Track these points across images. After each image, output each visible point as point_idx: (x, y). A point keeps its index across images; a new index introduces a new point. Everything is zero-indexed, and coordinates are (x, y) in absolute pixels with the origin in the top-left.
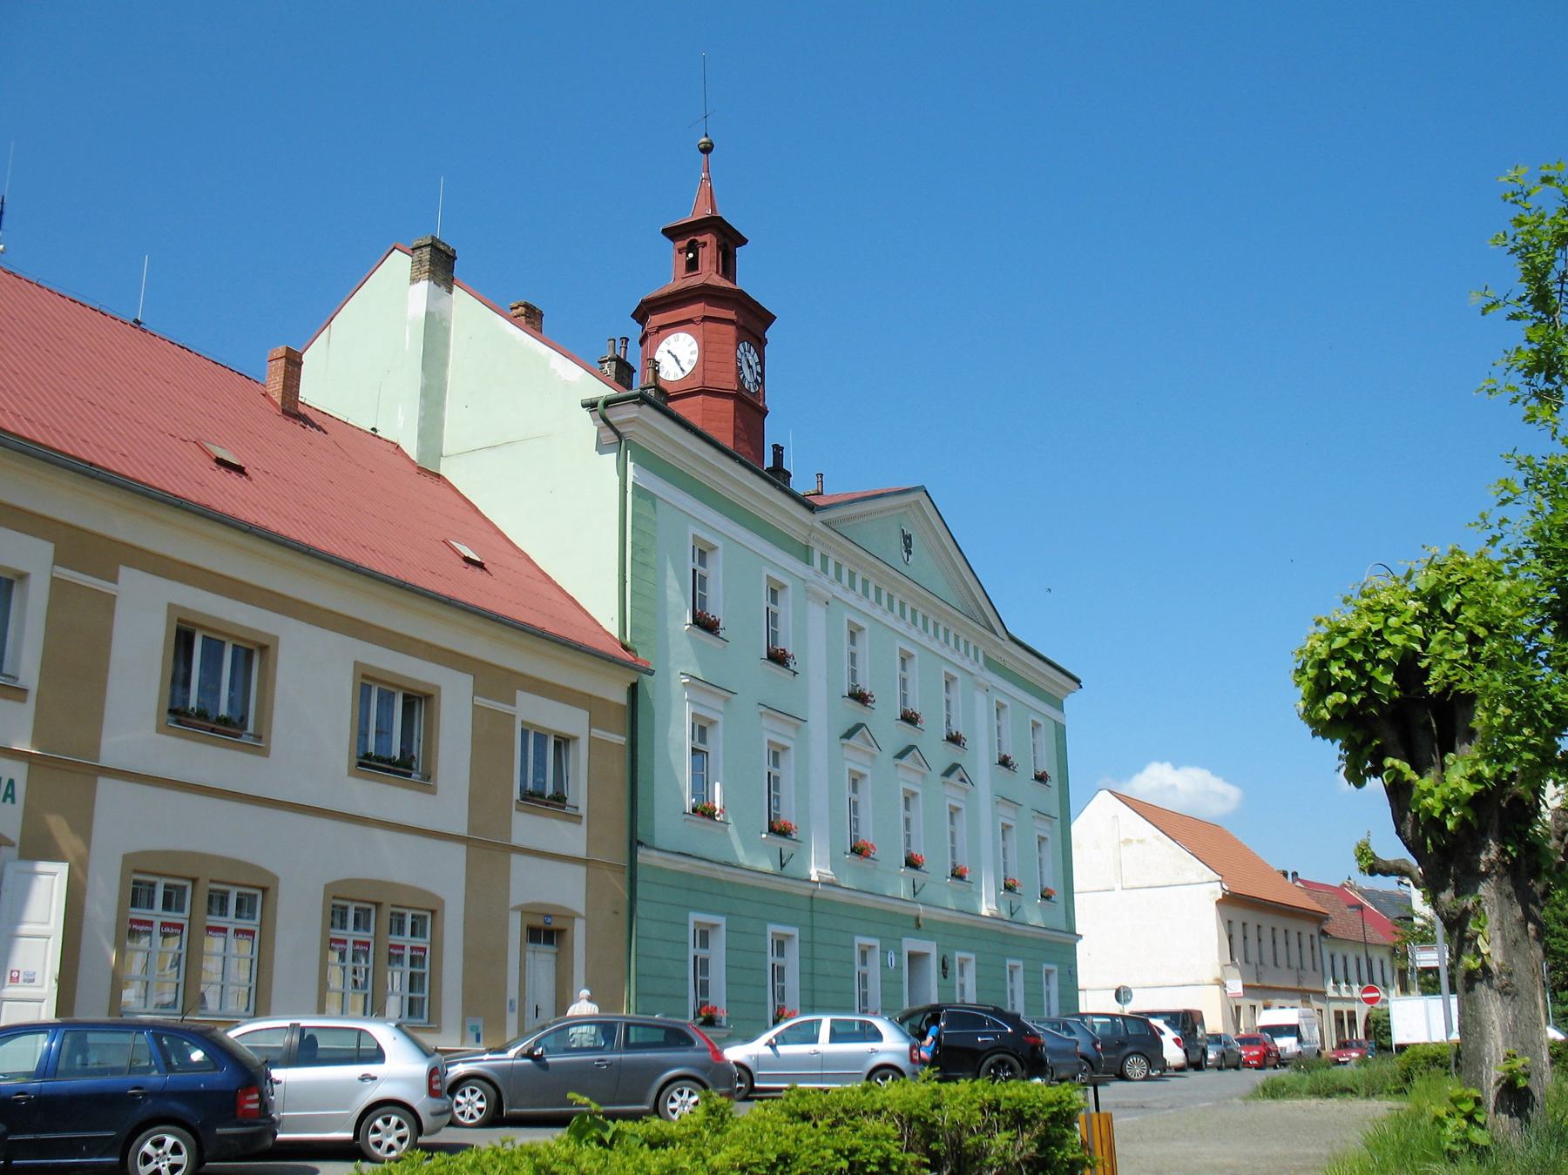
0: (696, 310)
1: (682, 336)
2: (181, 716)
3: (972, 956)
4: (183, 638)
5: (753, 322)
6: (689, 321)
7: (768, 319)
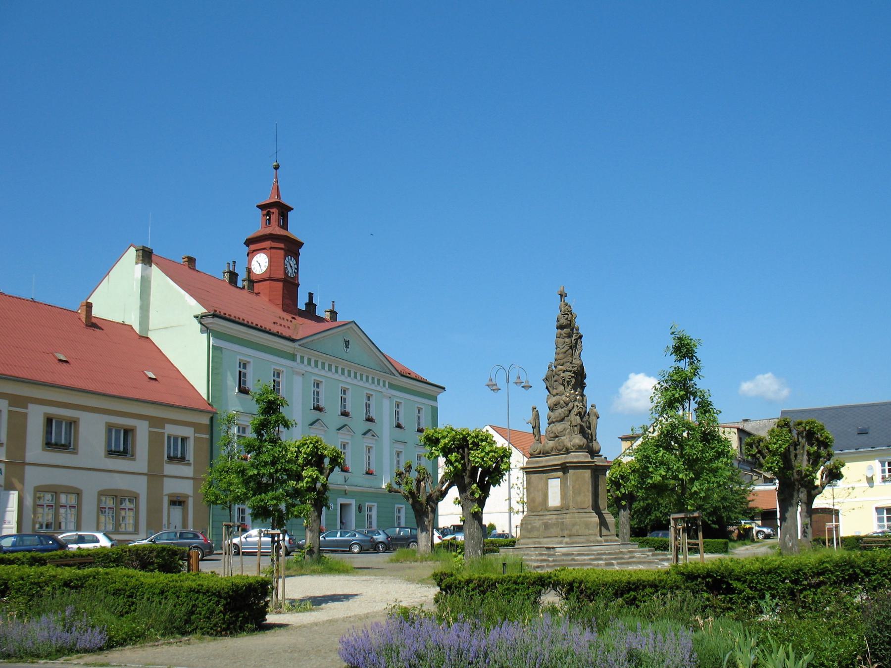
0: (268, 244)
1: (262, 255)
4: (49, 421)
5: (293, 247)
6: (265, 249)
7: (300, 244)
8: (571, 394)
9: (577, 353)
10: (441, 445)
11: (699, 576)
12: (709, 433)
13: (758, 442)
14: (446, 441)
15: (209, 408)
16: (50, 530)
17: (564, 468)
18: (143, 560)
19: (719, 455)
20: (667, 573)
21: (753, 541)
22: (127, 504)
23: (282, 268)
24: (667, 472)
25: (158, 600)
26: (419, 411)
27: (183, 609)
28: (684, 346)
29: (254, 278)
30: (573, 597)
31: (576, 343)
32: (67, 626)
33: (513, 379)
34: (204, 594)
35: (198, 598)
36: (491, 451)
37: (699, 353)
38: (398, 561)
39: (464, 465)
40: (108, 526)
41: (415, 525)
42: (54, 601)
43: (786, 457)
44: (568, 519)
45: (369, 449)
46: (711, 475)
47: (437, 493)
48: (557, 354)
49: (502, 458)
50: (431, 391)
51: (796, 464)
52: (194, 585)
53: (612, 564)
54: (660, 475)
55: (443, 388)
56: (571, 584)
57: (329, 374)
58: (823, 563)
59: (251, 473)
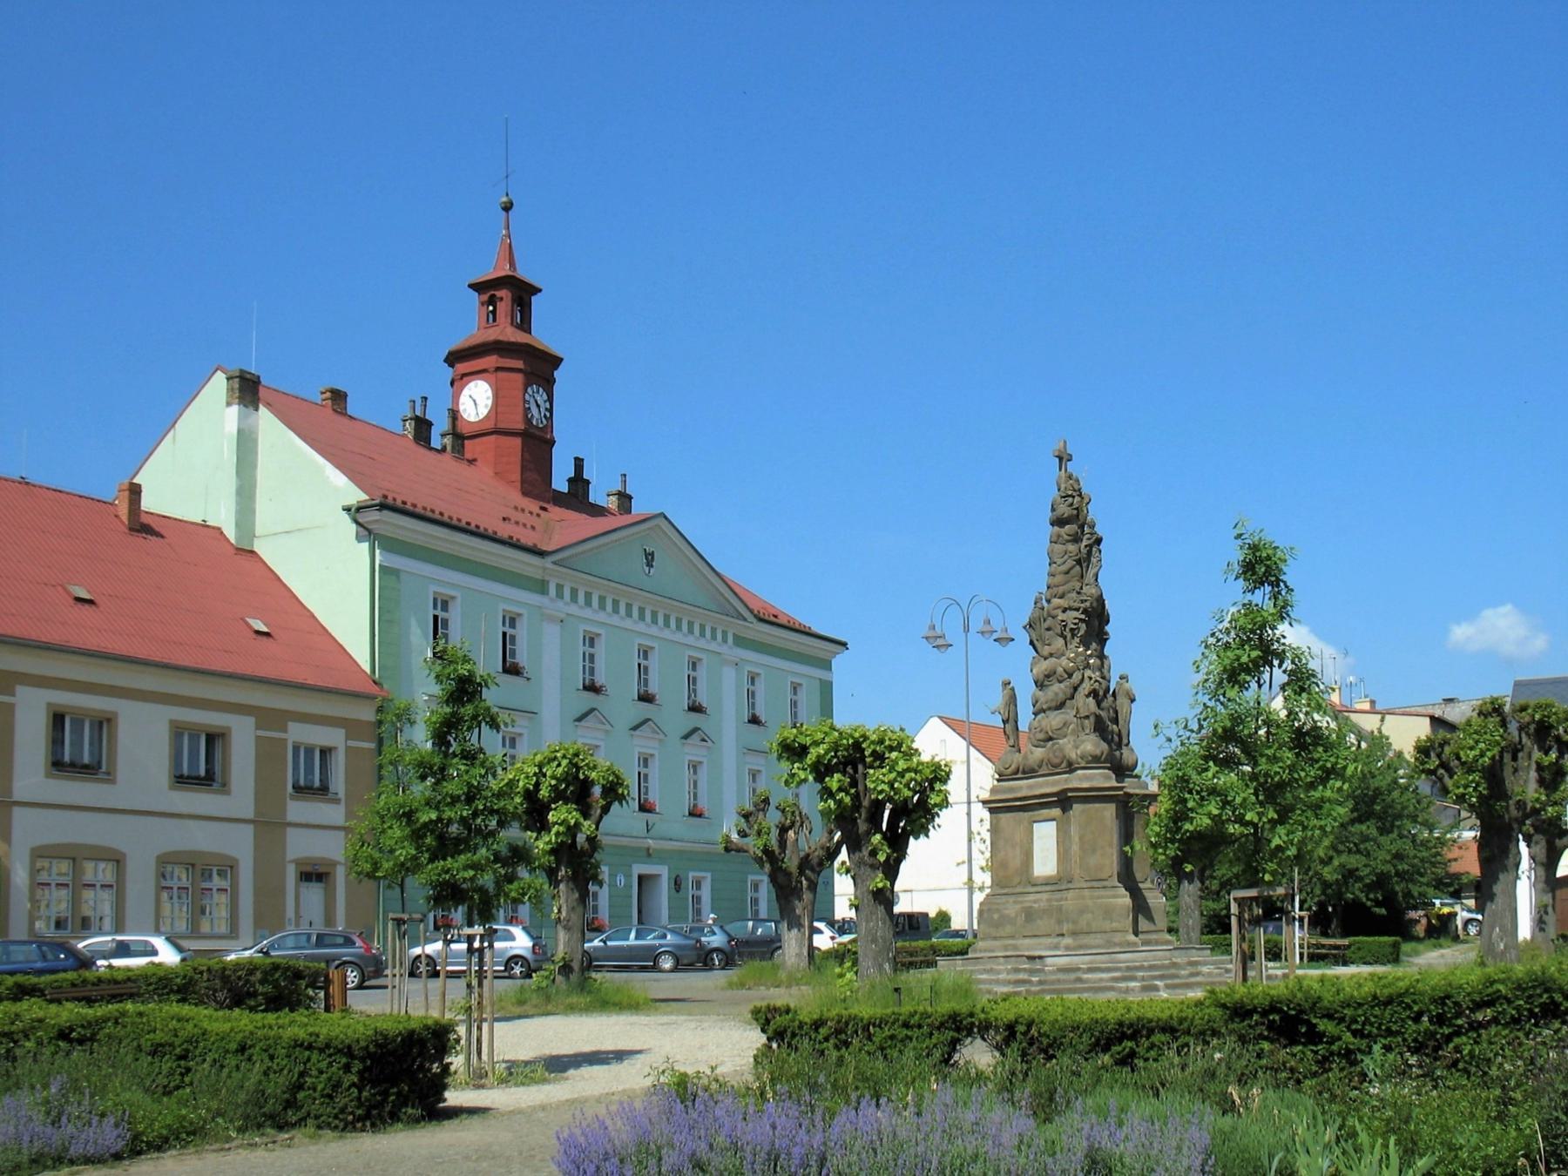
0: (491, 361)
3: (709, 875)
4: (58, 719)
5: (540, 367)
6: (484, 371)
7: (556, 361)
8: (1077, 654)
10: (811, 758)
11: (1254, 1010)
12: (1307, 733)
13: (1442, 746)
14: (821, 750)
15: (374, 689)
16: (61, 933)
17: (1064, 801)
18: (236, 989)
19: (1328, 774)
20: (1199, 1004)
21: (1456, 939)
22: (217, 882)
23: (520, 410)
24: (1223, 808)
25: (234, 1063)
26: (795, 688)
27: (281, 1080)
28: (1261, 561)
29: (465, 431)
30: (1013, 1051)
31: (1089, 553)
33: (976, 624)
34: (321, 1051)
35: (309, 1060)
36: (908, 770)
37: (1290, 575)
38: (742, 985)
39: (856, 798)
40: (177, 924)
41: (777, 916)
43: (1494, 775)
44: (1070, 900)
45: (694, 767)
46: (1309, 813)
47: (820, 853)
48: (1052, 575)
49: (932, 782)
50: (817, 650)
52: (302, 1034)
53: (1156, 989)
54: (1209, 814)
55: (844, 644)
56: (1011, 1028)
57: (615, 620)
58: (1493, 983)
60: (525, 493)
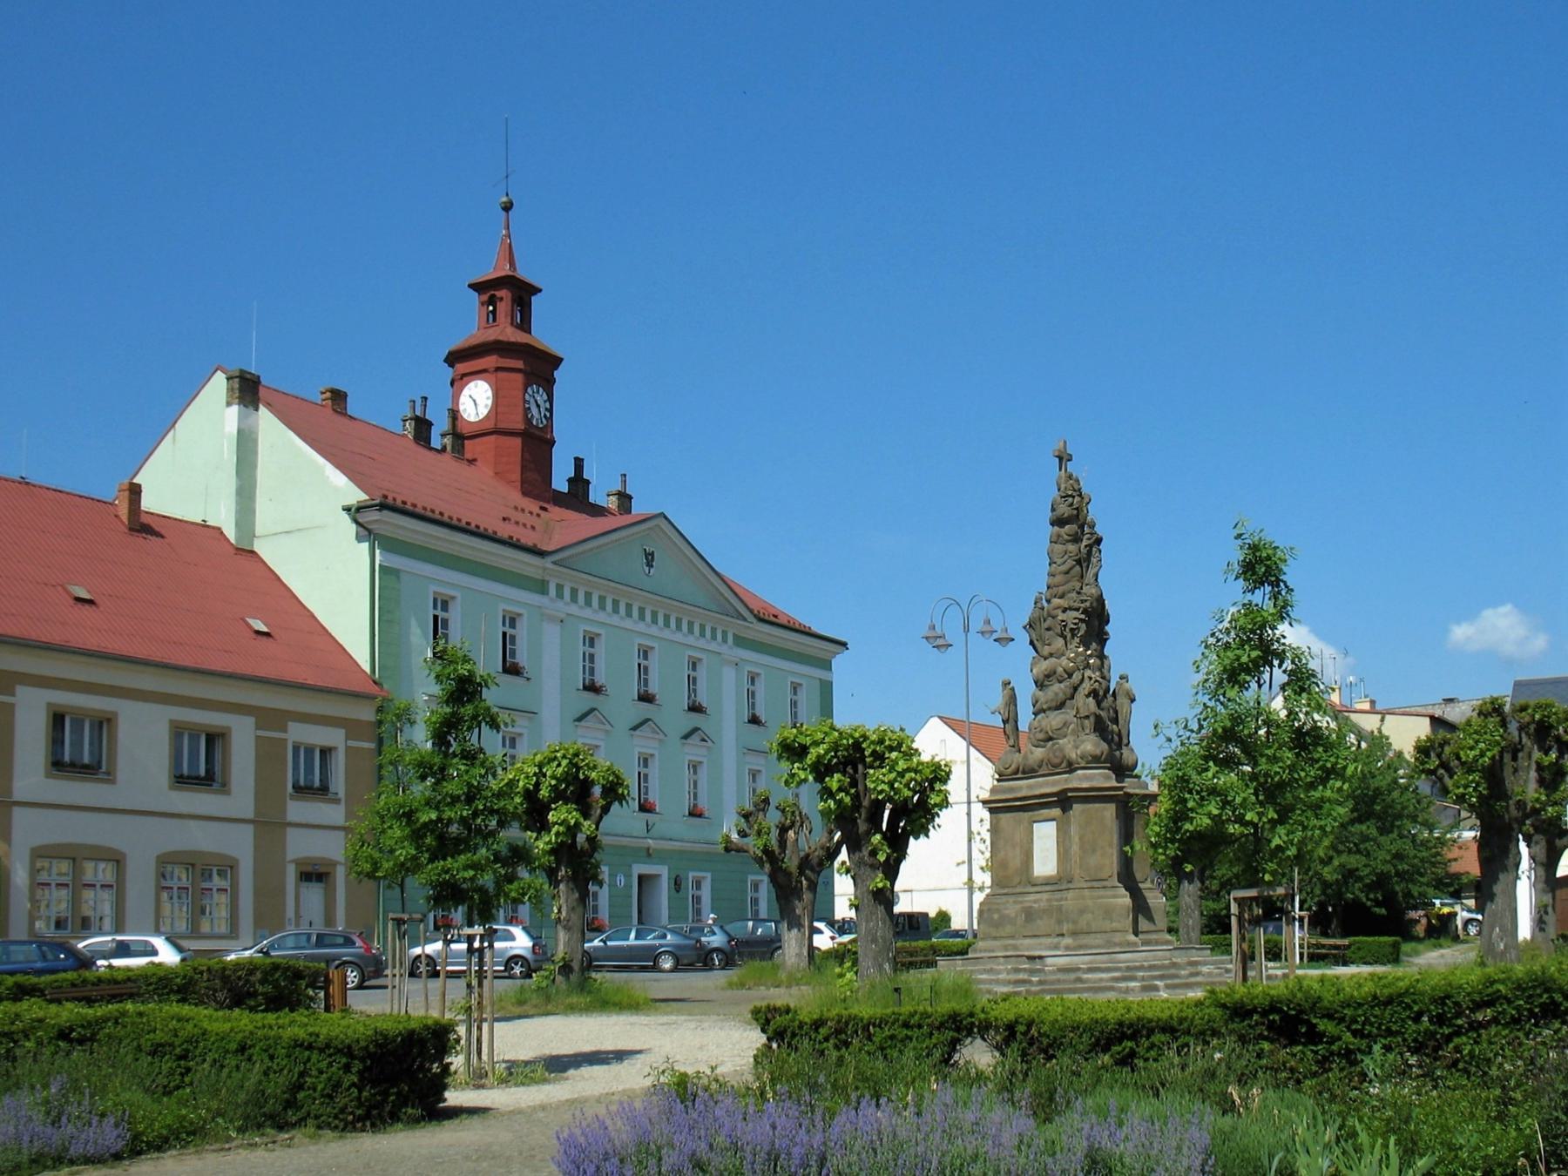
0: (491, 361)
2: (58, 765)
3: (709, 875)
4: (58, 719)
5: (540, 367)
6: (485, 371)
7: (556, 361)
9: (1091, 572)
10: (811, 758)
11: (1254, 1010)
12: (1308, 733)
15: (374, 689)
17: (1064, 801)
18: (236, 988)
19: (1328, 774)
20: (1199, 1004)
21: (1456, 939)
22: (217, 881)
23: (521, 410)
24: (1223, 808)
25: (234, 1063)
26: (795, 688)
27: (281, 1080)
28: (1261, 561)
29: (465, 431)
30: (1013, 1051)
31: (1089, 553)
32: (54, 1114)
33: (976, 624)
34: (321, 1051)
35: (309, 1059)
36: (908, 770)
37: (1290, 575)
38: (742, 985)
39: (856, 798)
40: (177, 924)
42: (36, 1068)
43: (1493, 775)
44: (1070, 900)
45: (695, 767)
46: (1309, 813)
47: (820, 853)
48: (1051, 575)
49: (932, 782)
50: (817, 650)
51: (1511, 783)
52: (301, 1034)
53: (1156, 989)
54: (1209, 814)
55: (844, 644)
56: (1011, 1028)
59: (424, 818)
60: (525, 493)
